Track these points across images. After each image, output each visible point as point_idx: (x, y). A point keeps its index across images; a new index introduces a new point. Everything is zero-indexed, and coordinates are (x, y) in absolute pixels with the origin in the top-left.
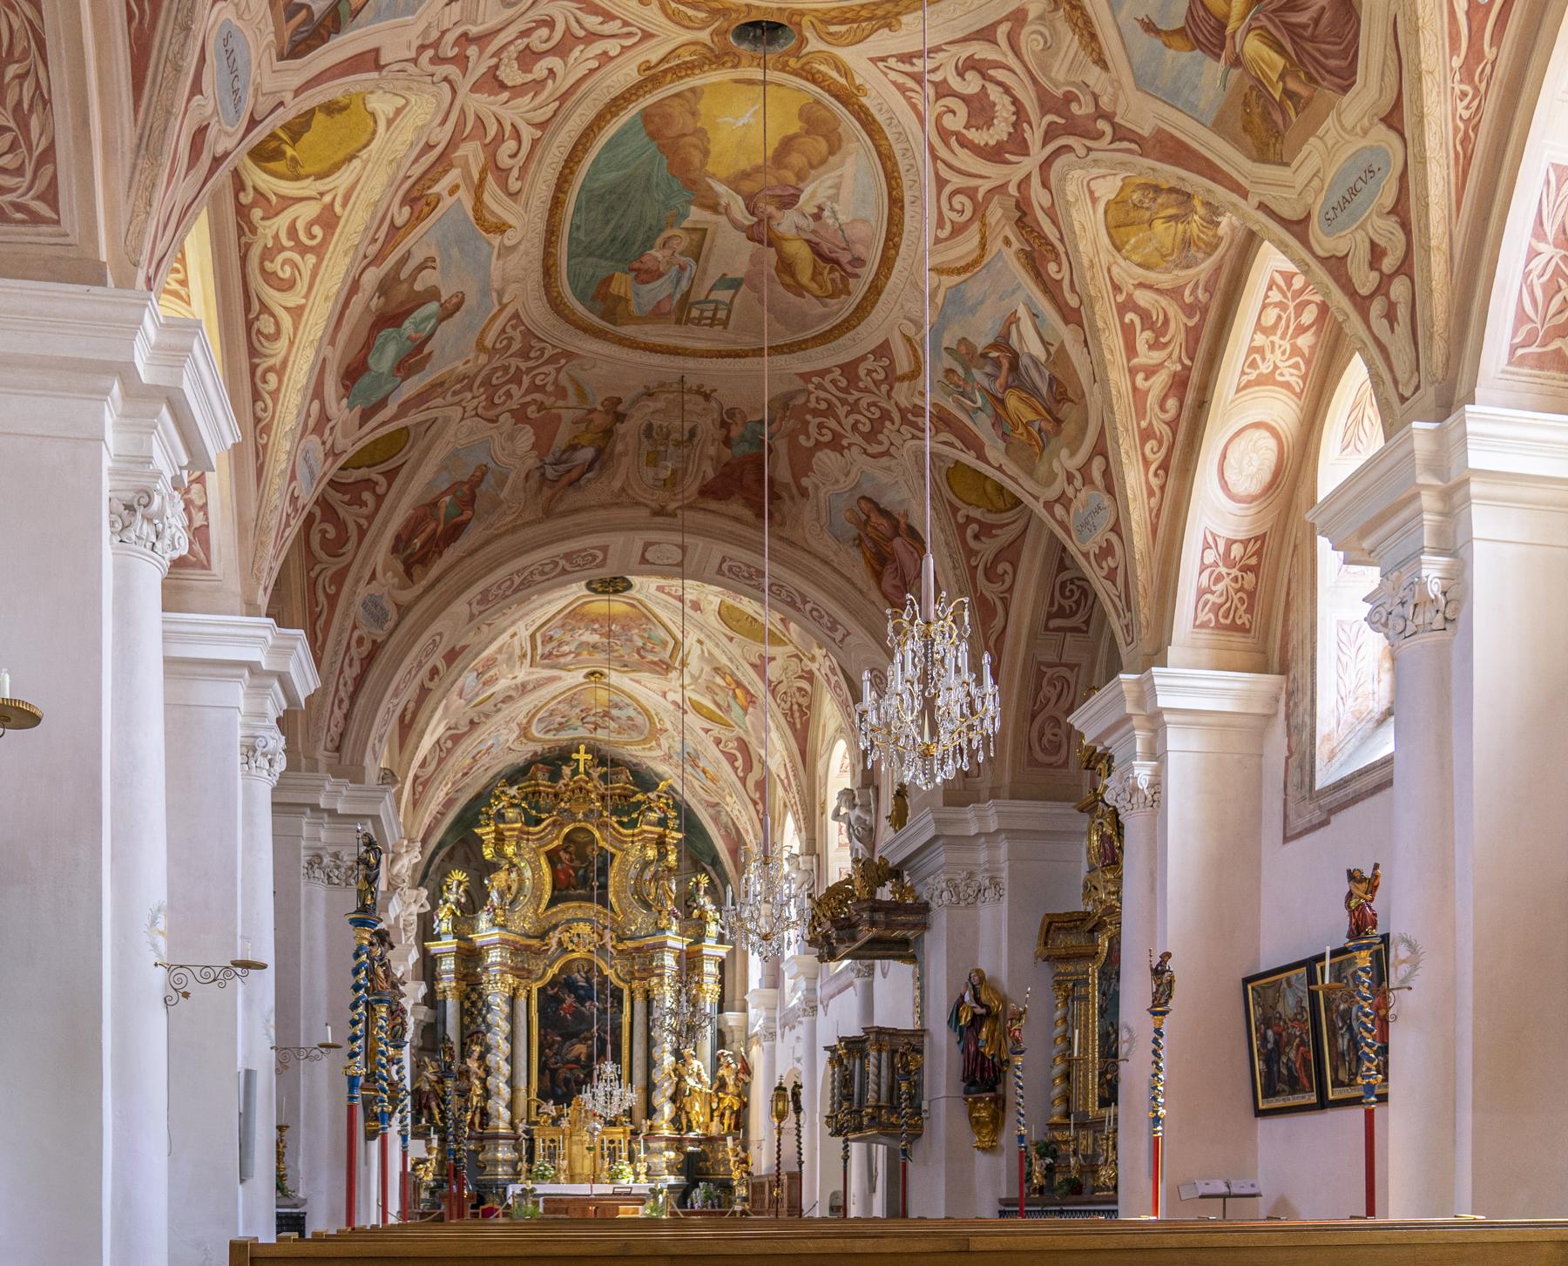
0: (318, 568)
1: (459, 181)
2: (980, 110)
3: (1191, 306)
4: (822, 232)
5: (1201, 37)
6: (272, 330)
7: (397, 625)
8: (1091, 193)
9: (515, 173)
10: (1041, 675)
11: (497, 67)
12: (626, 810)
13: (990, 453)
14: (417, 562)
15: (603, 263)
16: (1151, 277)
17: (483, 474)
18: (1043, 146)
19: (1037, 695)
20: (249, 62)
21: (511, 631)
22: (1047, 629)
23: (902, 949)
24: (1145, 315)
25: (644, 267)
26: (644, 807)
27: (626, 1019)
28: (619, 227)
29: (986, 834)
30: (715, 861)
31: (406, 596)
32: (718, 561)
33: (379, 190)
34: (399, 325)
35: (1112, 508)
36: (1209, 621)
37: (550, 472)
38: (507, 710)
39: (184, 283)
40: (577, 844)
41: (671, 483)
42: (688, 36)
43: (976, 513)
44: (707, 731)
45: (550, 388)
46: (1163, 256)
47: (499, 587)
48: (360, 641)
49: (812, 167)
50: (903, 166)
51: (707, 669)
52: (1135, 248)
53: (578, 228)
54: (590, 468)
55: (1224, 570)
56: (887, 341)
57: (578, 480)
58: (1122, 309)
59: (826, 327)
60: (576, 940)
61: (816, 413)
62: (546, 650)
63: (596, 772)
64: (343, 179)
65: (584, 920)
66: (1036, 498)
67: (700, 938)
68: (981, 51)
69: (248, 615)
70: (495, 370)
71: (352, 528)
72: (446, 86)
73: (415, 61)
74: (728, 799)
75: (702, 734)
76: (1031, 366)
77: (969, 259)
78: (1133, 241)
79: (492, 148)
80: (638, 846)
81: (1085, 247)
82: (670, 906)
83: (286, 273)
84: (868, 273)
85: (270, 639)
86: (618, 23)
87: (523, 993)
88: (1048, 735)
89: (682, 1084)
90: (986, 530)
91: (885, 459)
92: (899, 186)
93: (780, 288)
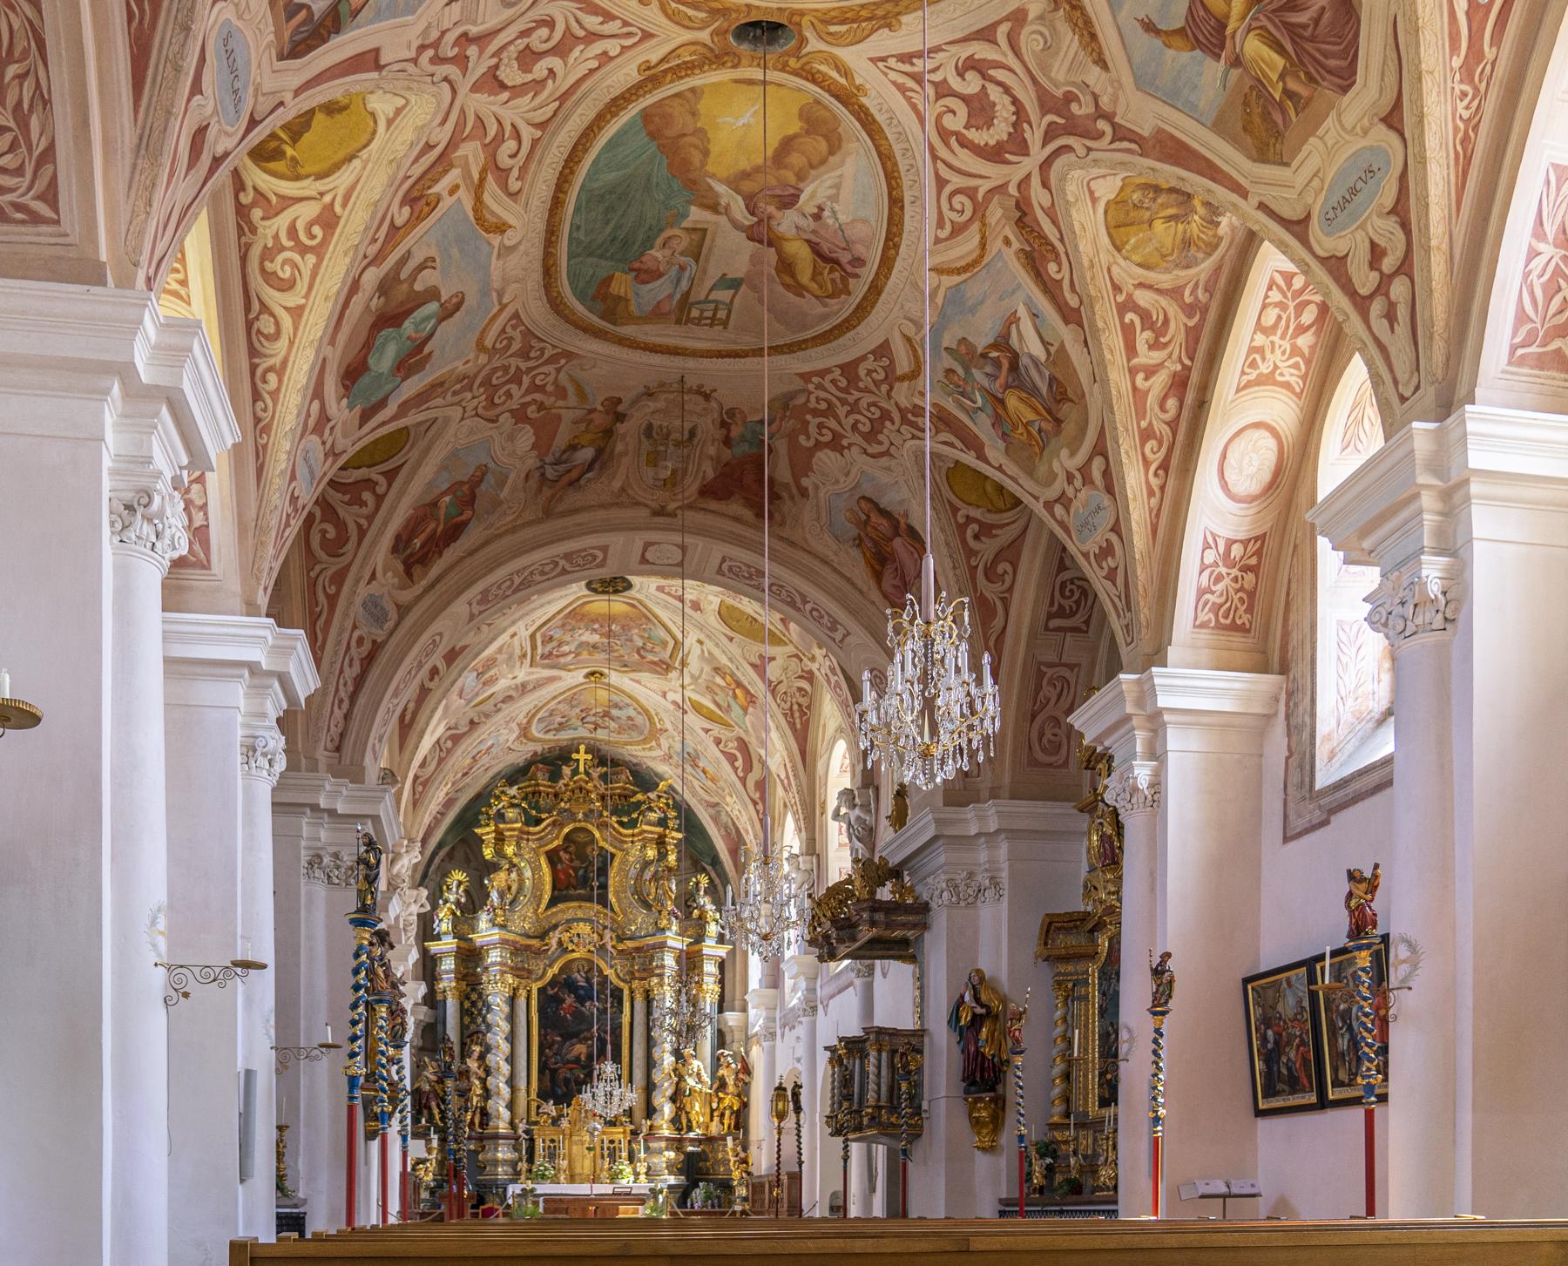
0: (318, 568)
1: (459, 181)
2: (980, 110)
3: (1191, 306)
4: (822, 232)
5: (1201, 37)
6: (272, 330)
7: (397, 625)
8: (1091, 193)
9: (515, 173)
10: (1041, 675)
11: (497, 67)
12: (626, 810)
13: (990, 453)
14: (417, 562)
15: (603, 263)
16: (1151, 277)
17: (483, 474)
18: (1043, 146)
19: (1037, 695)
20: (249, 62)
21: (511, 631)
22: (1047, 629)
23: (902, 949)
24: (1145, 315)
25: (644, 267)
26: (644, 807)
27: (626, 1019)
28: (619, 227)
29: (986, 834)
30: (715, 861)
31: (406, 596)
32: (718, 561)
33: (379, 190)
34: (399, 325)
35: (1112, 508)
36: (1209, 621)
37: (550, 472)
38: (507, 710)
39: (184, 283)
40: (577, 844)
41: (671, 483)
42: (688, 36)
43: (976, 513)
44: (707, 731)
45: (550, 388)
46: (1163, 256)
47: (499, 587)
48: (360, 641)
49: (812, 167)
50: (903, 166)
51: (707, 669)
52: (1135, 248)
53: (578, 228)
54: (590, 468)
55: (1224, 570)
56: (887, 341)
57: (578, 480)
58: (1122, 309)
59: (826, 327)
60: (576, 940)
61: (816, 413)
62: (546, 650)
63: (596, 772)
64: (343, 179)
65: (584, 920)
66: (1036, 498)
67: (700, 938)
68: (981, 51)
69: (248, 615)
70: (495, 370)
71: (352, 528)
72: (446, 86)
73: (415, 61)
74: (728, 799)
75: (702, 734)
76: (1031, 366)
77: (969, 259)
78: (1133, 241)
79: (492, 148)
80: (638, 846)
81: (1085, 247)
82: (670, 906)
83: (286, 273)
84: (868, 273)
85: (270, 639)
86: (618, 23)
87: (523, 993)
88: (1048, 735)
89: (682, 1084)
90: (986, 530)
91: (885, 459)
92: (899, 186)
93: (780, 288)
